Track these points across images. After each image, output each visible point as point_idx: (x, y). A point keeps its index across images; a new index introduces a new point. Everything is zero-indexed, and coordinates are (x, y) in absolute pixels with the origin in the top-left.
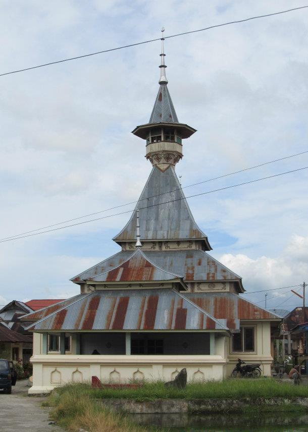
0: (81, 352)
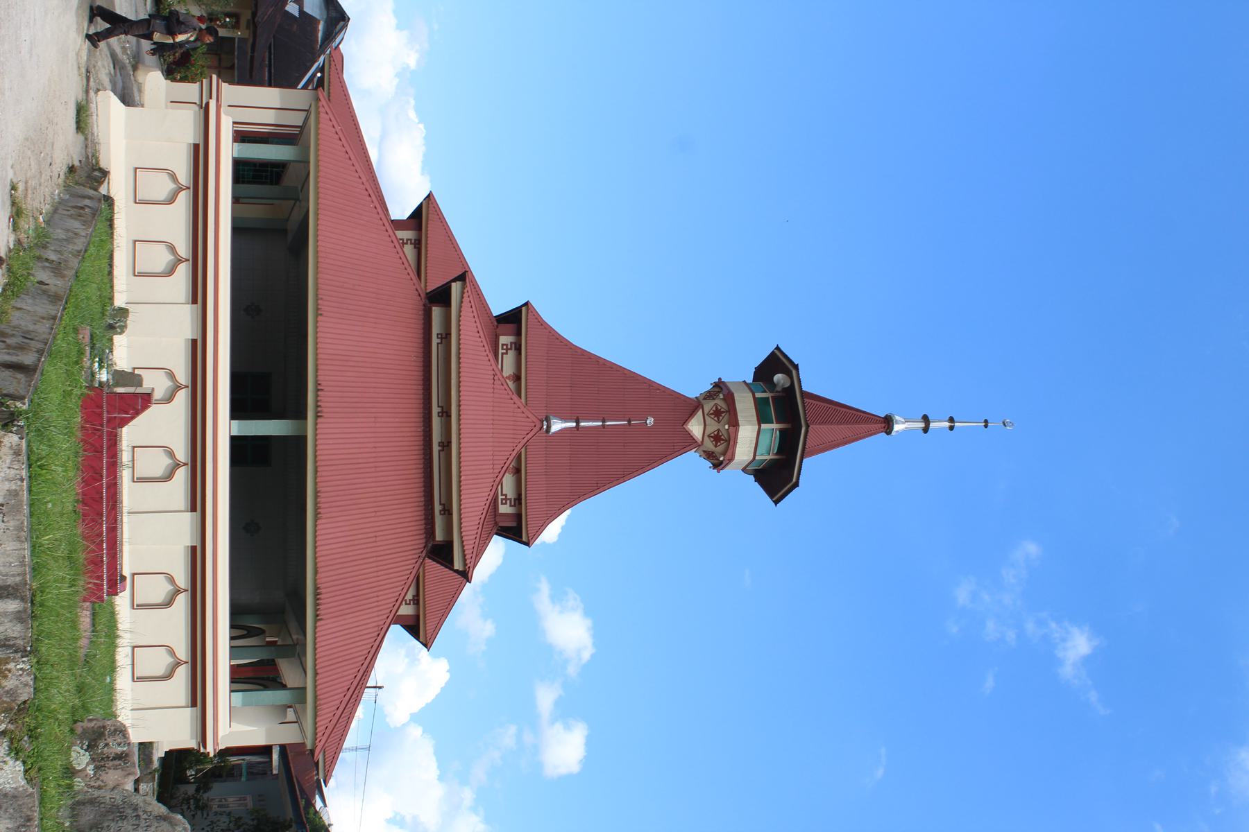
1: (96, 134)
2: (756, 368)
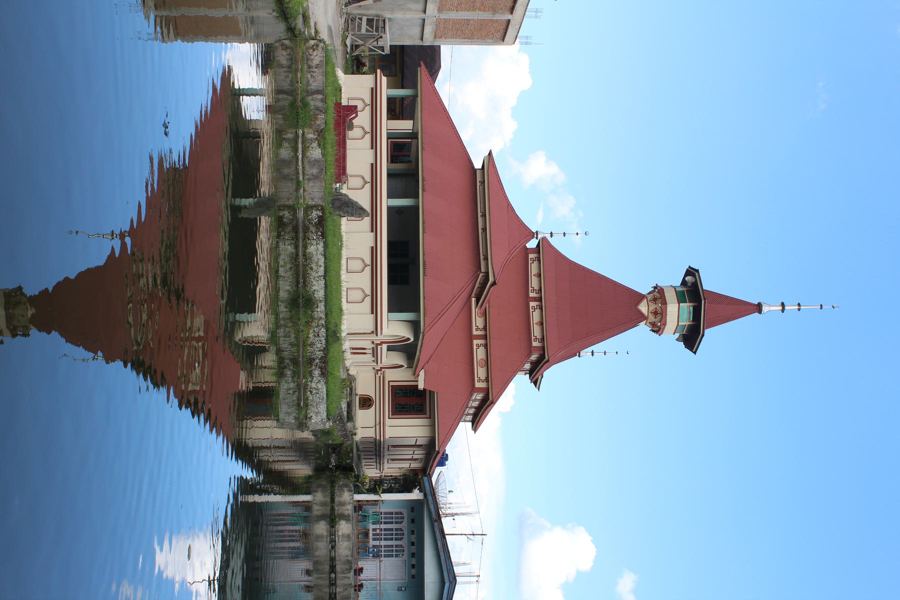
0: (389, 175)
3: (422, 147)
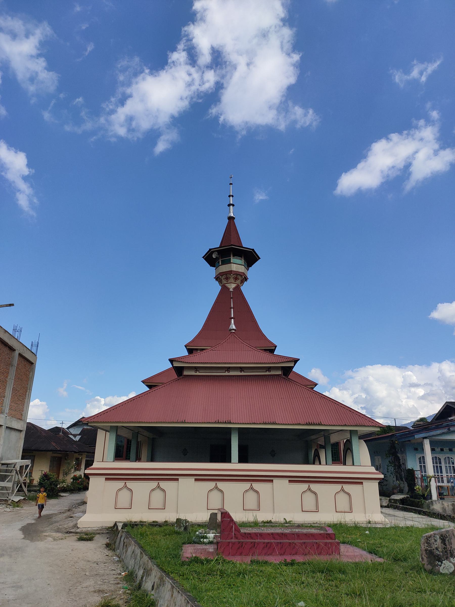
1: (98, 528)
2: (210, 266)
3: (182, 422)
